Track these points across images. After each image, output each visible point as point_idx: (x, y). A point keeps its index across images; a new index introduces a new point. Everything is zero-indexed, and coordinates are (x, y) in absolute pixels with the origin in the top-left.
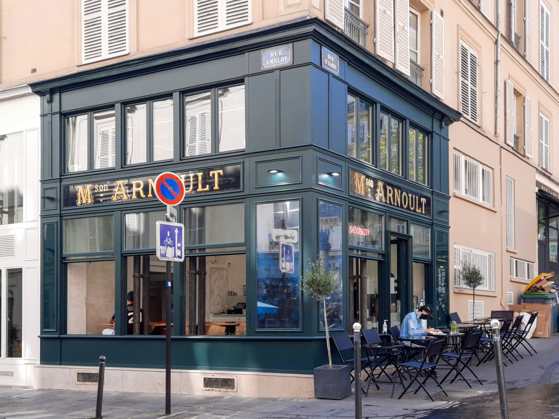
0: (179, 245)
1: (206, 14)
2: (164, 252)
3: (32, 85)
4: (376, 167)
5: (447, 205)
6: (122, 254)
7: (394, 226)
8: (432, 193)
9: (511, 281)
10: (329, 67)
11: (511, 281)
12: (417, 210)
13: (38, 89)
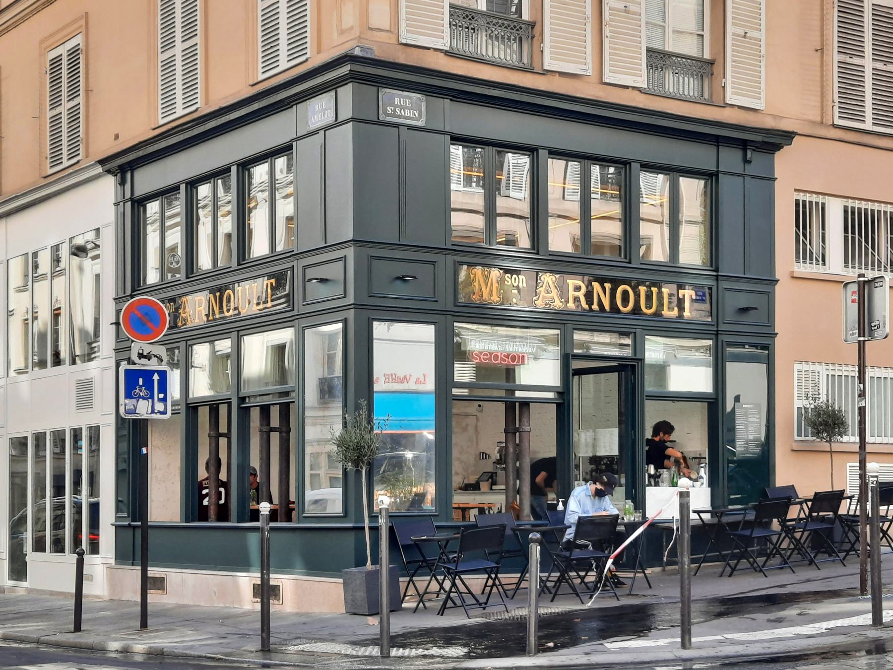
0: (161, 396)
1: (268, 47)
2: (132, 407)
3: (102, 162)
4: (538, 253)
5: (770, 297)
6: (187, 404)
7: (604, 344)
8: (717, 278)
9: (793, 277)
10: (399, 117)
11: (793, 277)
12: (666, 313)
13: (108, 167)
